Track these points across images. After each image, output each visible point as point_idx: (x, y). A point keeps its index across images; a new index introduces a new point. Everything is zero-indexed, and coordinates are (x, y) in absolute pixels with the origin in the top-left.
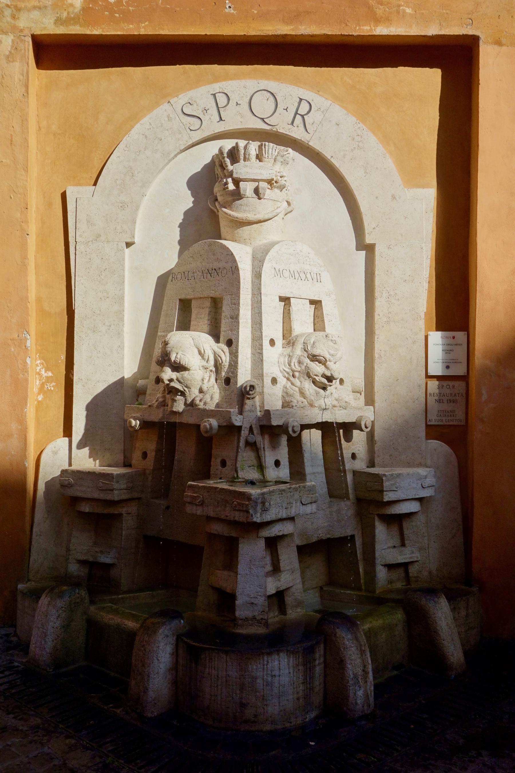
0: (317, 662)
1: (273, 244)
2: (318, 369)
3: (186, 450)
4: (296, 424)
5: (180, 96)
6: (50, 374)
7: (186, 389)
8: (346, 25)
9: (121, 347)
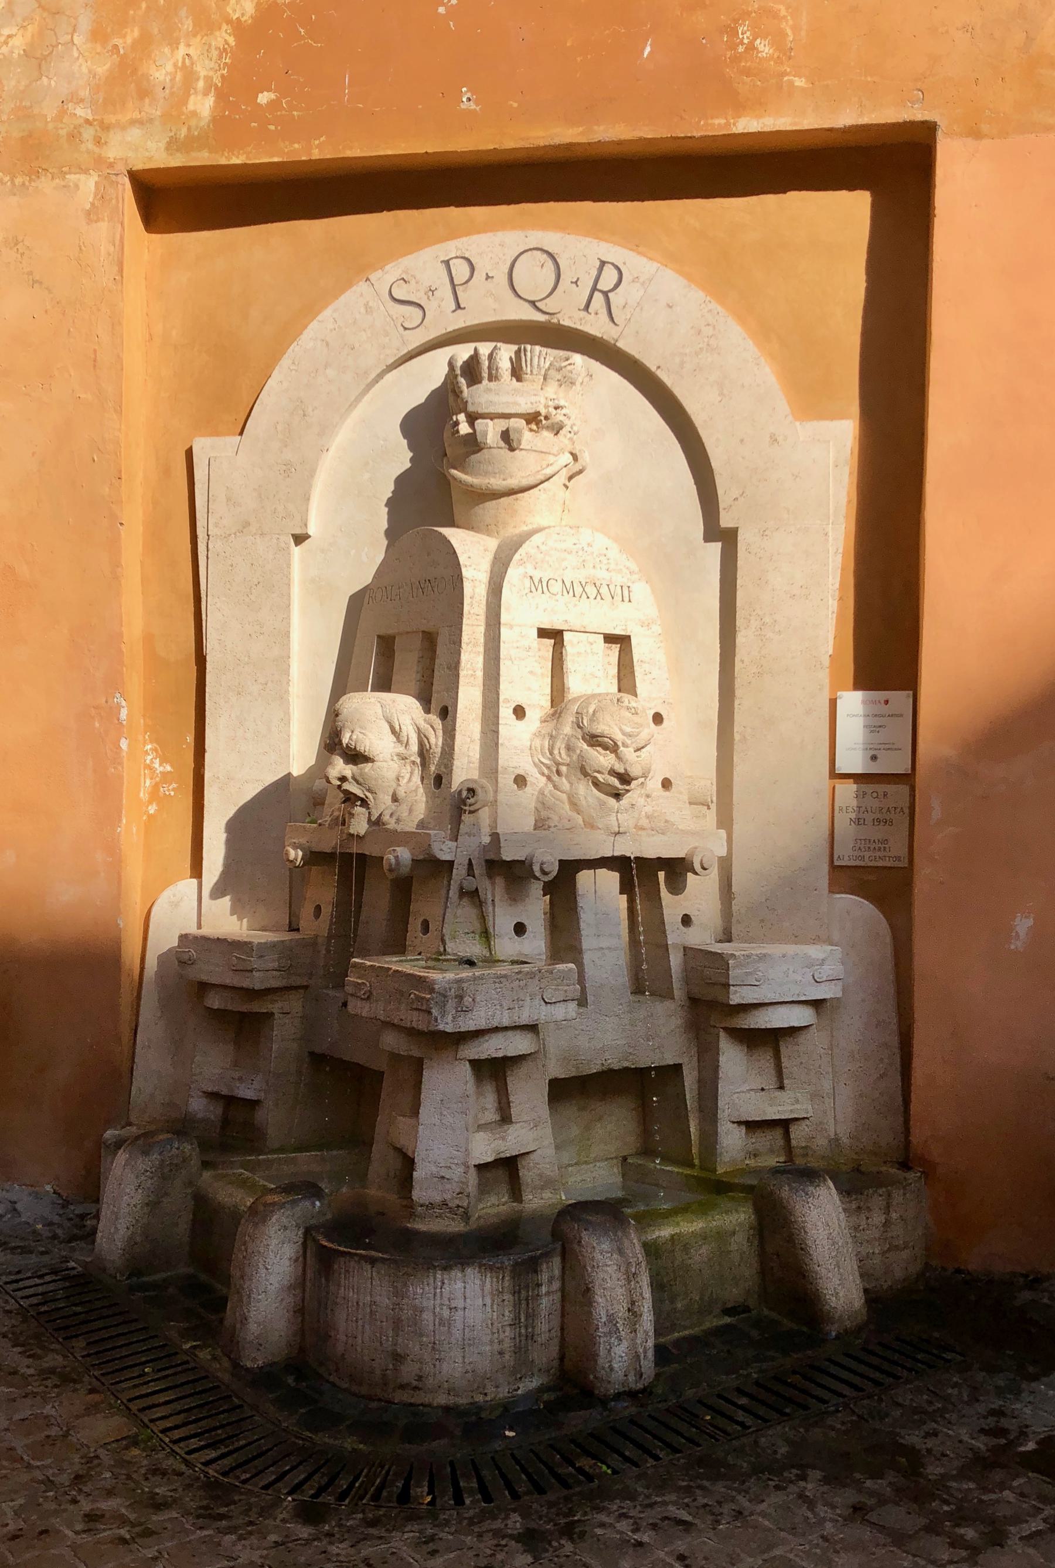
0: (544, 1289)
1: (529, 535)
2: (603, 760)
3: (377, 903)
4: (547, 858)
5: (387, 268)
6: (169, 768)
7: (368, 794)
8: (681, 118)
9: (286, 720)
